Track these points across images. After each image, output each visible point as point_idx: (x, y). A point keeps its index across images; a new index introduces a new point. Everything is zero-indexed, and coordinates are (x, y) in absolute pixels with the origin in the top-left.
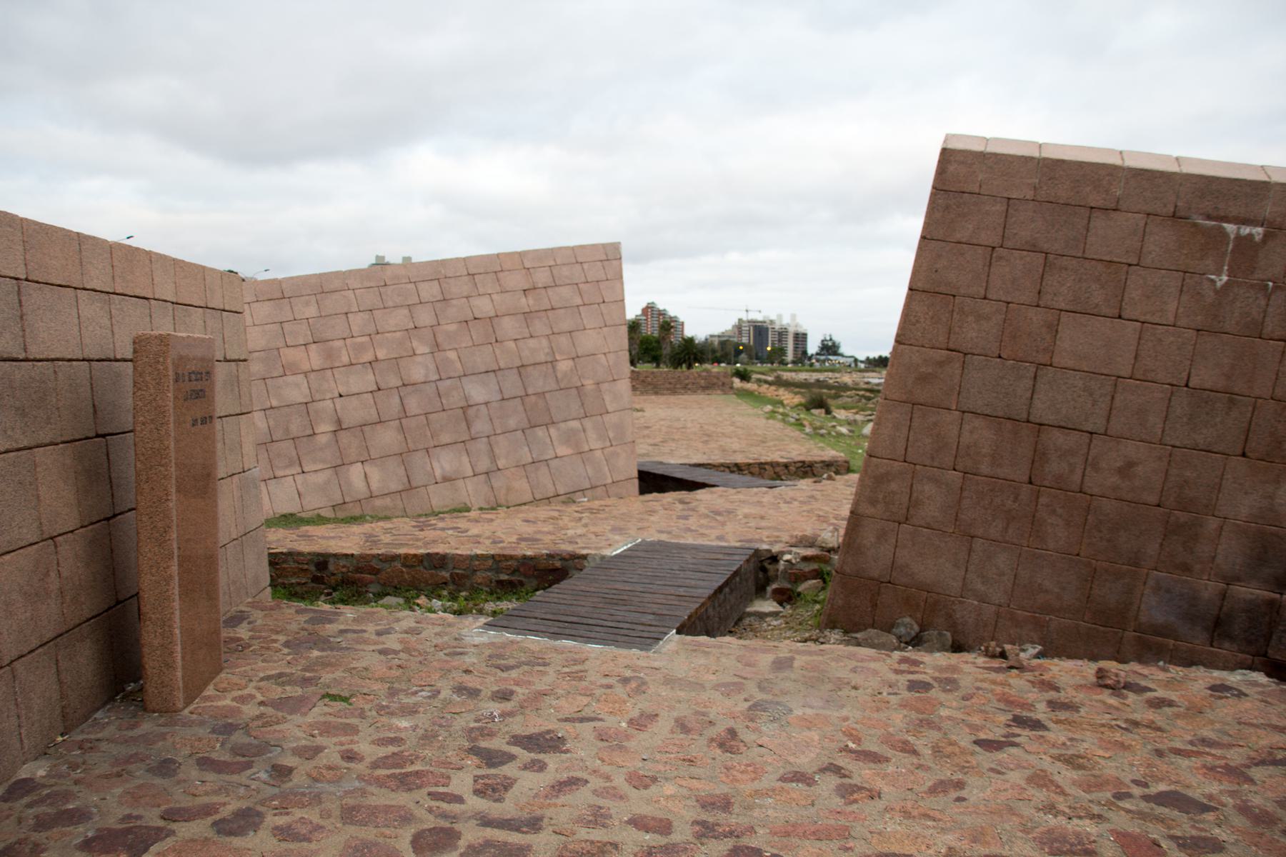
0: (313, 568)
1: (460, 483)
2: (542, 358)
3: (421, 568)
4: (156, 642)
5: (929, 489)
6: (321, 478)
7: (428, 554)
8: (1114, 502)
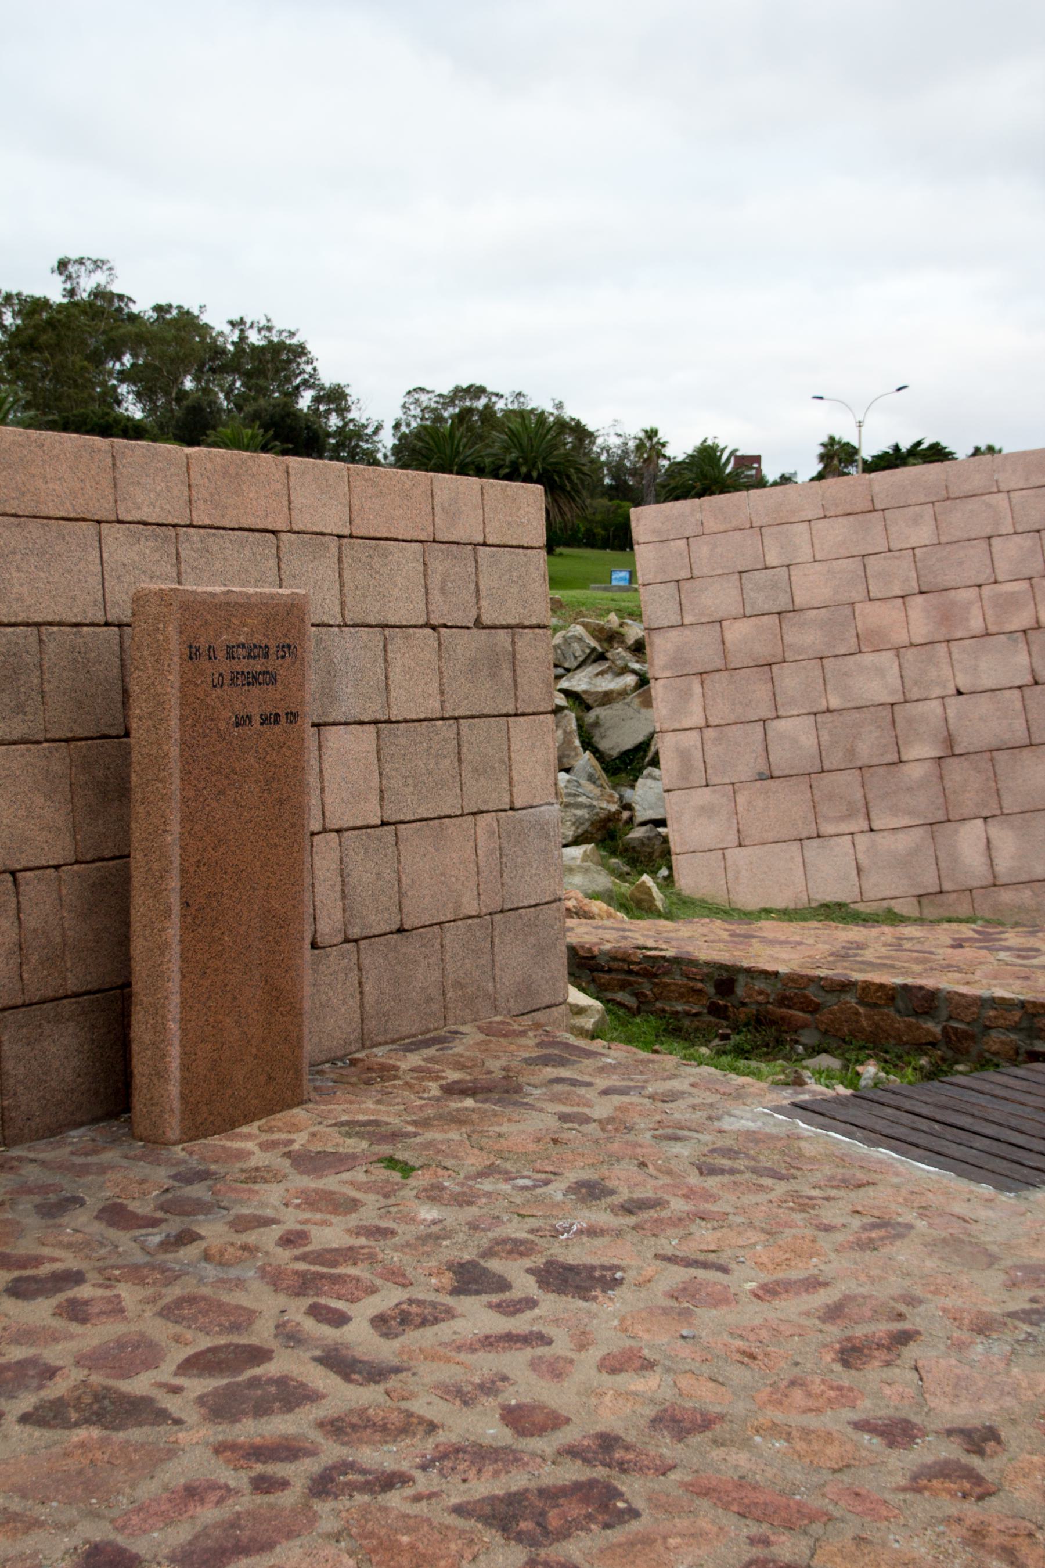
0: (711, 990)
3: (891, 1011)
4: (147, 1037)
6: (902, 843)
7: (905, 987)
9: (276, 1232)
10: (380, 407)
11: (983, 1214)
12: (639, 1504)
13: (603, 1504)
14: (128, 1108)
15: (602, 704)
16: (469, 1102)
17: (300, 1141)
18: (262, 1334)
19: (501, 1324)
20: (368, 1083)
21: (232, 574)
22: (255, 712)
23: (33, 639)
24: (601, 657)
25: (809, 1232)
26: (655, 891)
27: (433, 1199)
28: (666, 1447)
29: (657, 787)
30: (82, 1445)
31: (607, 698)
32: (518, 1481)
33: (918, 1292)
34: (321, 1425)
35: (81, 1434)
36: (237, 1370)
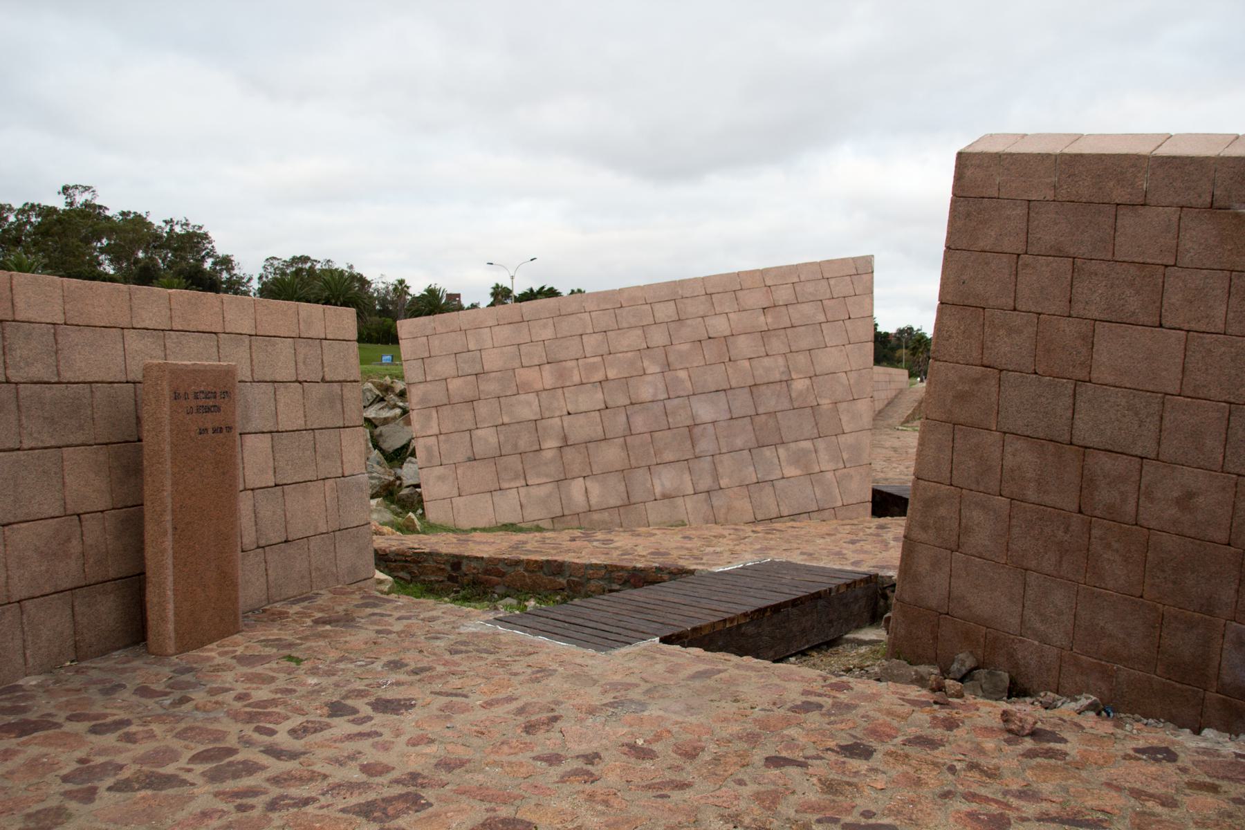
0: (449, 568)
1: (679, 501)
2: (778, 377)
3: (541, 574)
4: (155, 600)
5: (977, 515)
6: (543, 491)
7: (548, 561)
8: (1175, 538)
9: (232, 694)
10: (251, 266)
11: (590, 662)
12: (432, 800)
13: (415, 802)
14: (144, 639)
15: (383, 424)
16: (328, 627)
17: (240, 650)
18: (231, 741)
19: (356, 729)
20: (273, 620)
21: (192, 355)
22: (210, 426)
23: (88, 390)
24: (382, 400)
25: (507, 677)
26: (416, 520)
27: (314, 674)
28: (443, 776)
29: (415, 467)
30: (143, 798)
31: (386, 421)
32: (371, 796)
33: (561, 699)
34: (268, 780)
35: (142, 793)
36: (221, 760)
